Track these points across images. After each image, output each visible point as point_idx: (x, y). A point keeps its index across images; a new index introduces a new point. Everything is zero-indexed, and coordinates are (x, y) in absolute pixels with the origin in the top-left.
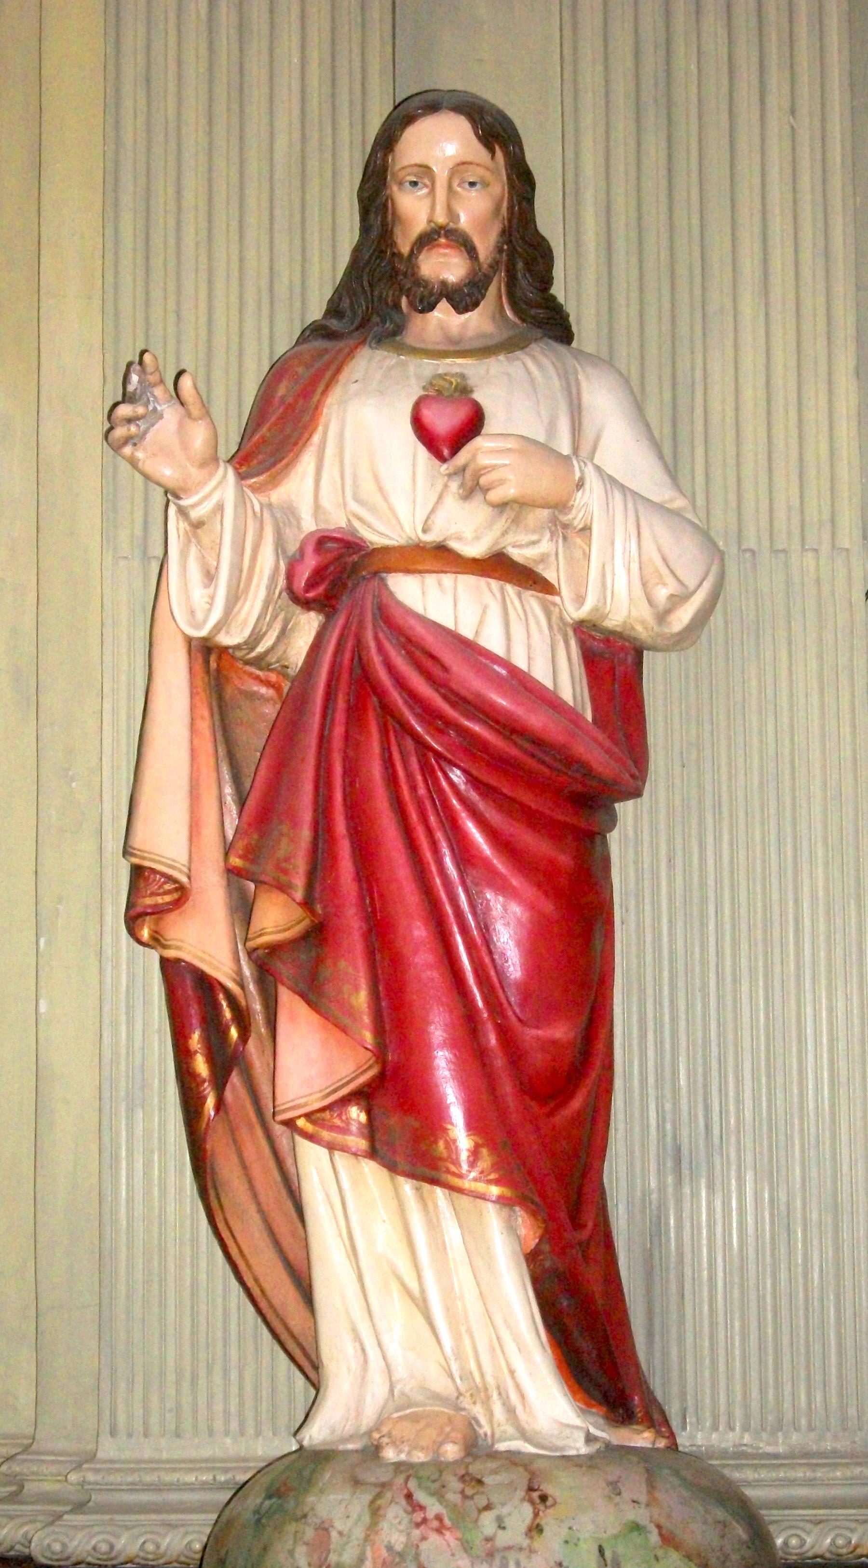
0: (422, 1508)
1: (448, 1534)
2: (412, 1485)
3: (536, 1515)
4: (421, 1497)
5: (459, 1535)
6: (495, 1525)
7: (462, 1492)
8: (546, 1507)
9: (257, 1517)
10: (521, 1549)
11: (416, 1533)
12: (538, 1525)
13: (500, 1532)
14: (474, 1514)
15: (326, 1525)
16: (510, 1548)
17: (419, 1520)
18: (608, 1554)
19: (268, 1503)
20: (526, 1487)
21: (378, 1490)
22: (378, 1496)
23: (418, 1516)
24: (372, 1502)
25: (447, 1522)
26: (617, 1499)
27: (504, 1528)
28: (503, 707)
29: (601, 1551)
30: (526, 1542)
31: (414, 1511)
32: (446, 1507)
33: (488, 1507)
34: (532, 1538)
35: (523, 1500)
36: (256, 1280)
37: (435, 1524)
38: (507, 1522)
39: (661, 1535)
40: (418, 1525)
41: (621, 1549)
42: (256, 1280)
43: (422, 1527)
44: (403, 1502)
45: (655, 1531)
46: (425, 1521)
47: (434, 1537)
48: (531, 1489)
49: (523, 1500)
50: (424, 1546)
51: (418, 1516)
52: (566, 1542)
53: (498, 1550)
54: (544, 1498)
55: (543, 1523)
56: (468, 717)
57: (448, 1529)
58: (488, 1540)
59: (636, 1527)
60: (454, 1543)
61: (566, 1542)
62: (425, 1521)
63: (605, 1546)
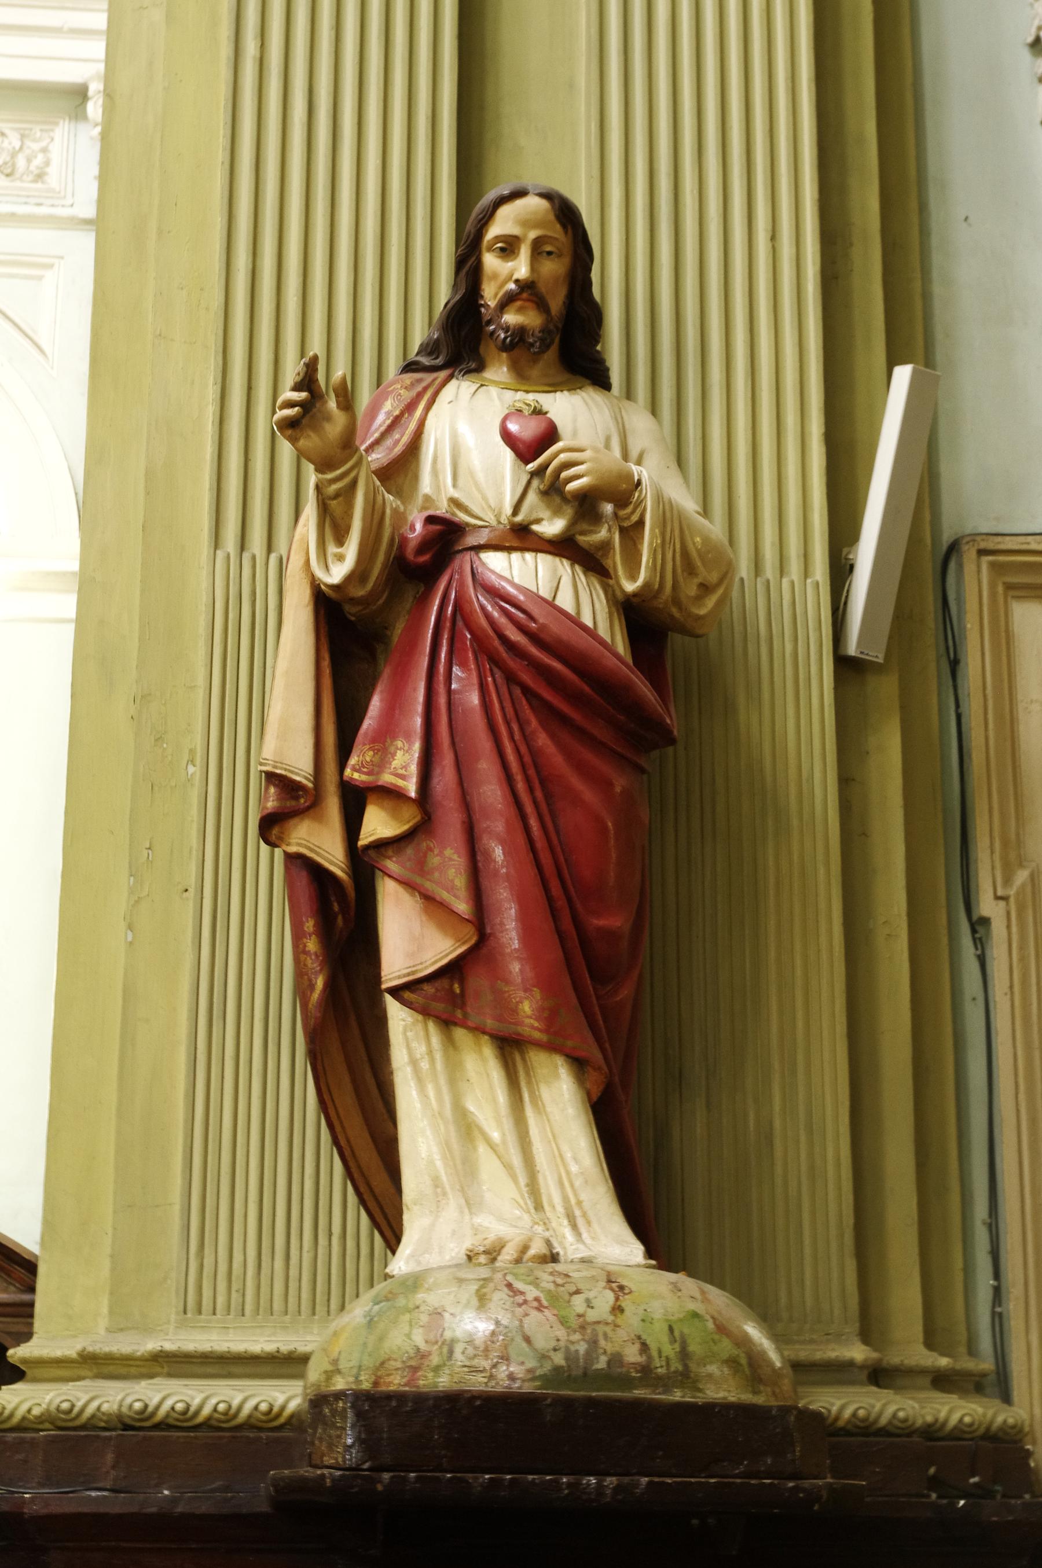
0: (522, 1293)
1: (547, 1312)
2: (509, 1278)
3: (617, 1299)
4: (519, 1285)
5: (555, 1312)
6: (585, 1305)
7: (554, 1282)
8: (625, 1294)
9: (368, 1318)
10: (607, 1324)
11: (519, 1311)
12: (620, 1306)
13: (589, 1310)
14: (567, 1297)
15: (439, 1311)
16: (599, 1322)
17: (521, 1301)
18: (677, 1334)
19: (377, 1307)
20: (605, 1278)
21: (482, 1283)
22: (482, 1287)
23: (520, 1299)
24: (478, 1291)
25: (545, 1303)
26: (679, 1294)
27: (592, 1308)
28: (363, 782)
29: (671, 1329)
30: (610, 1318)
31: (515, 1295)
32: (542, 1292)
33: (578, 1292)
34: (615, 1315)
35: (605, 1288)
36: (348, 1141)
37: (535, 1304)
38: (594, 1303)
39: (715, 1323)
40: (520, 1305)
41: (686, 1331)
42: (348, 1141)
43: (524, 1307)
44: (506, 1289)
45: (711, 1320)
46: (525, 1302)
47: (534, 1313)
48: (609, 1281)
49: (605, 1288)
50: (526, 1321)
51: (520, 1299)
52: (643, 1320)
53: (589, 1324)
54: (621, 1288)
55: (623, 1305)
56: (449, 600)
57: (546, 1307)
58: (579, 1316)
59: (695, 1315)
60: (552, 1318)
61: (643, 1320)
62: (525, 1302)
63: (675, 1327)
